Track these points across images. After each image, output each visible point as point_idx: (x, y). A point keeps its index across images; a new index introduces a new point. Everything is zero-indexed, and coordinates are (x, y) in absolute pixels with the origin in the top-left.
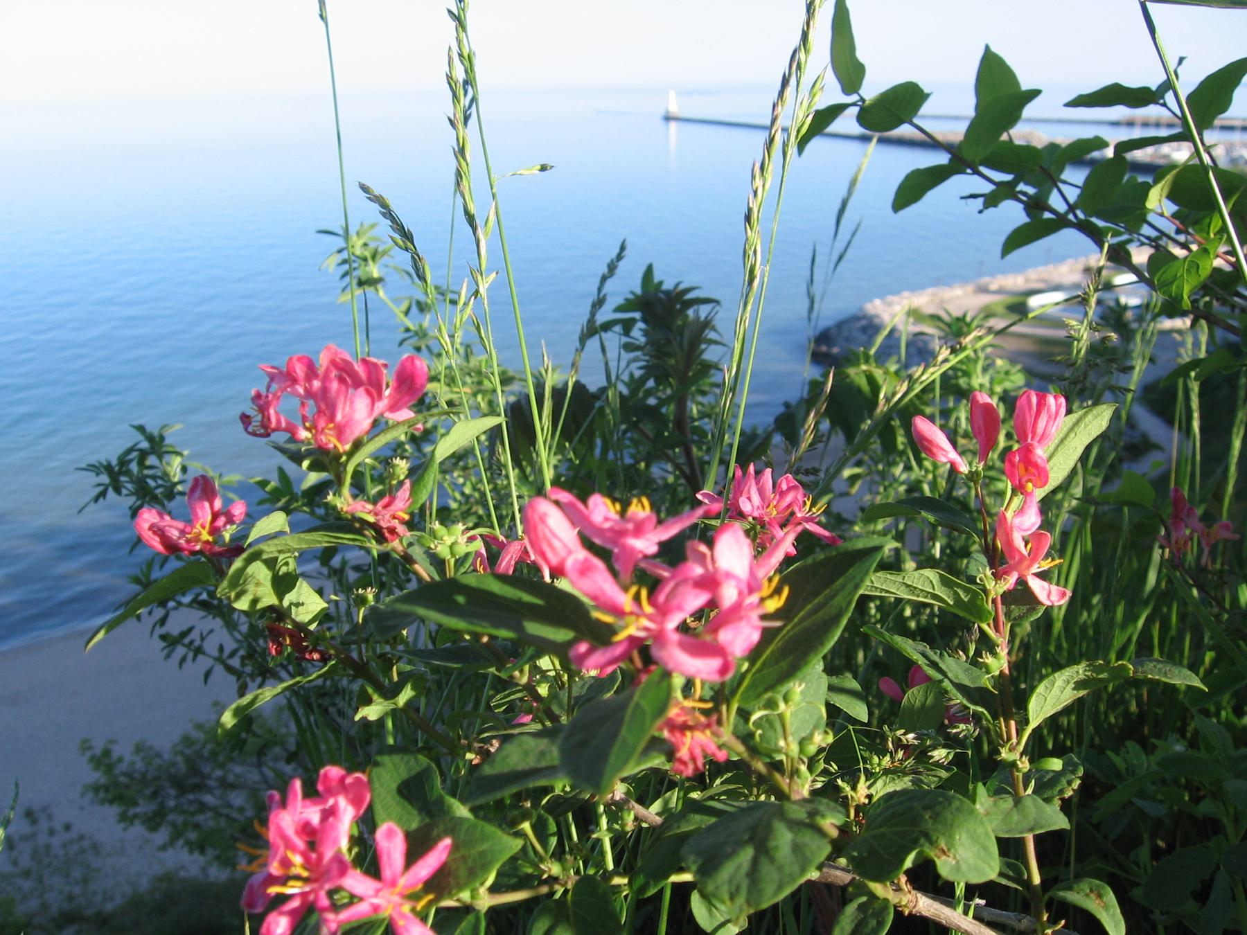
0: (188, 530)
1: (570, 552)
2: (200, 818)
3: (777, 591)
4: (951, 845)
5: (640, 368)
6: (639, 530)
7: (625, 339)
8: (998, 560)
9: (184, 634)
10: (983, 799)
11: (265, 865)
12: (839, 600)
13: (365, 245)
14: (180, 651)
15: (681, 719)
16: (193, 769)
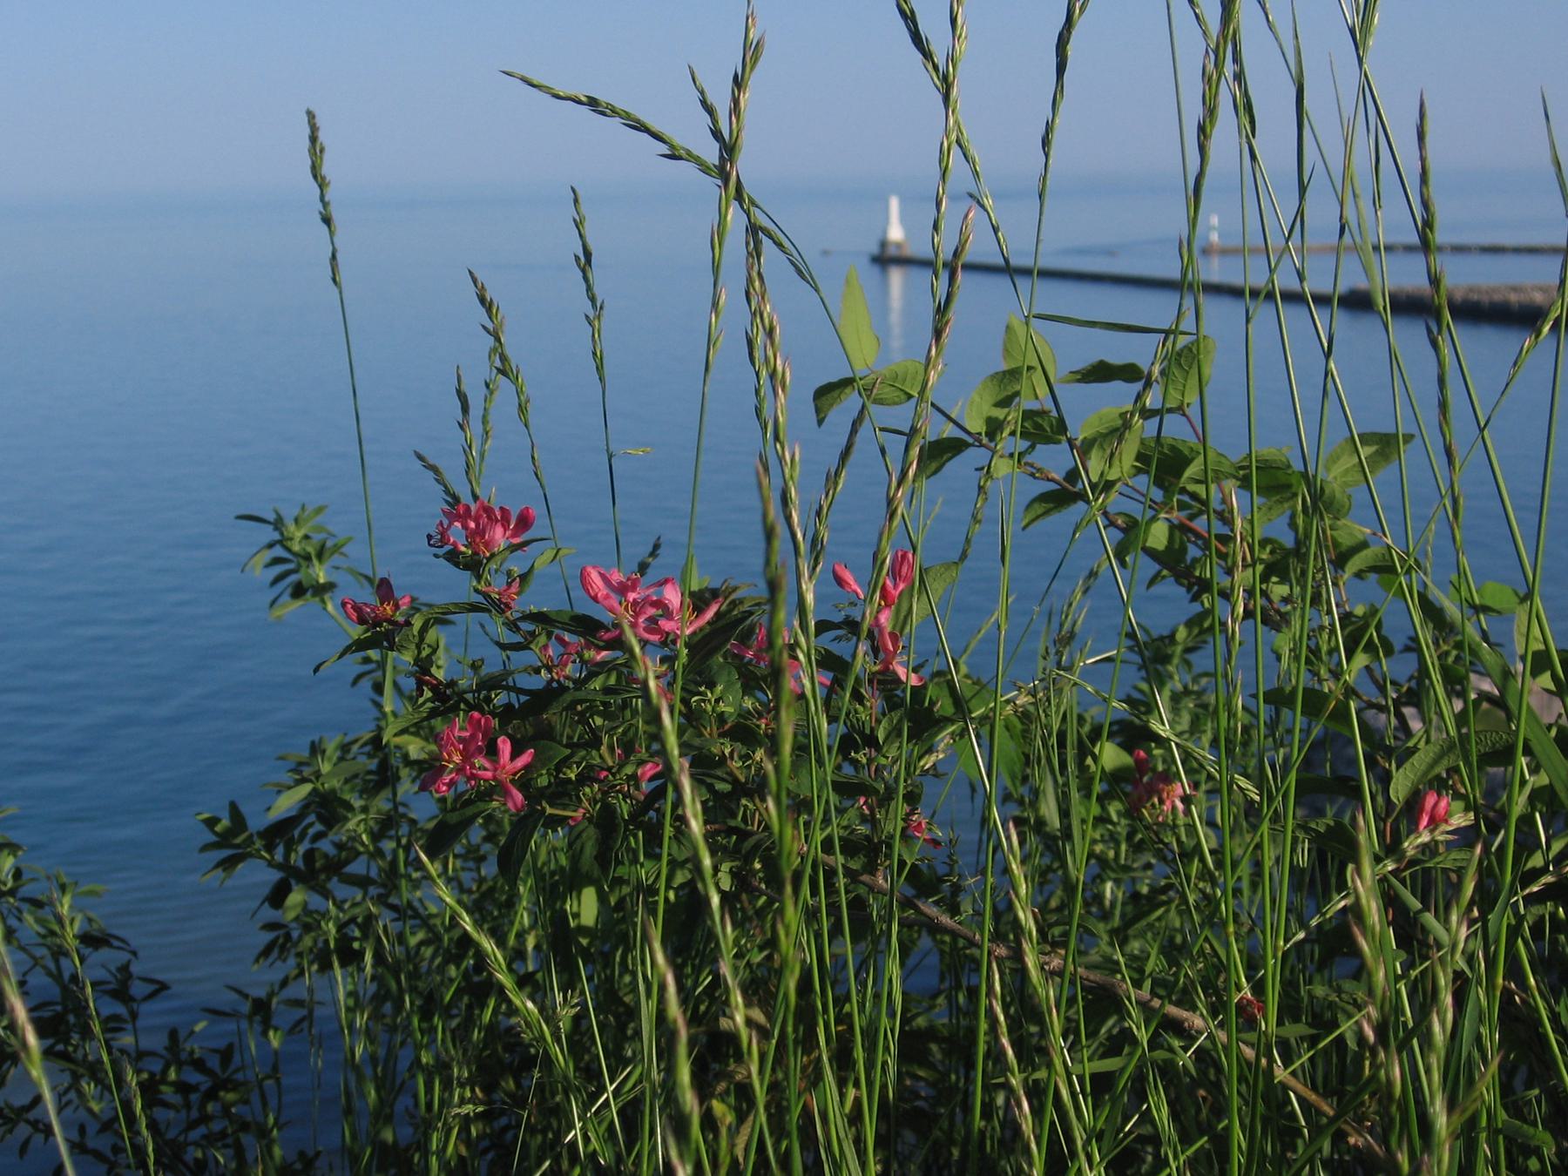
13: (306, 537)
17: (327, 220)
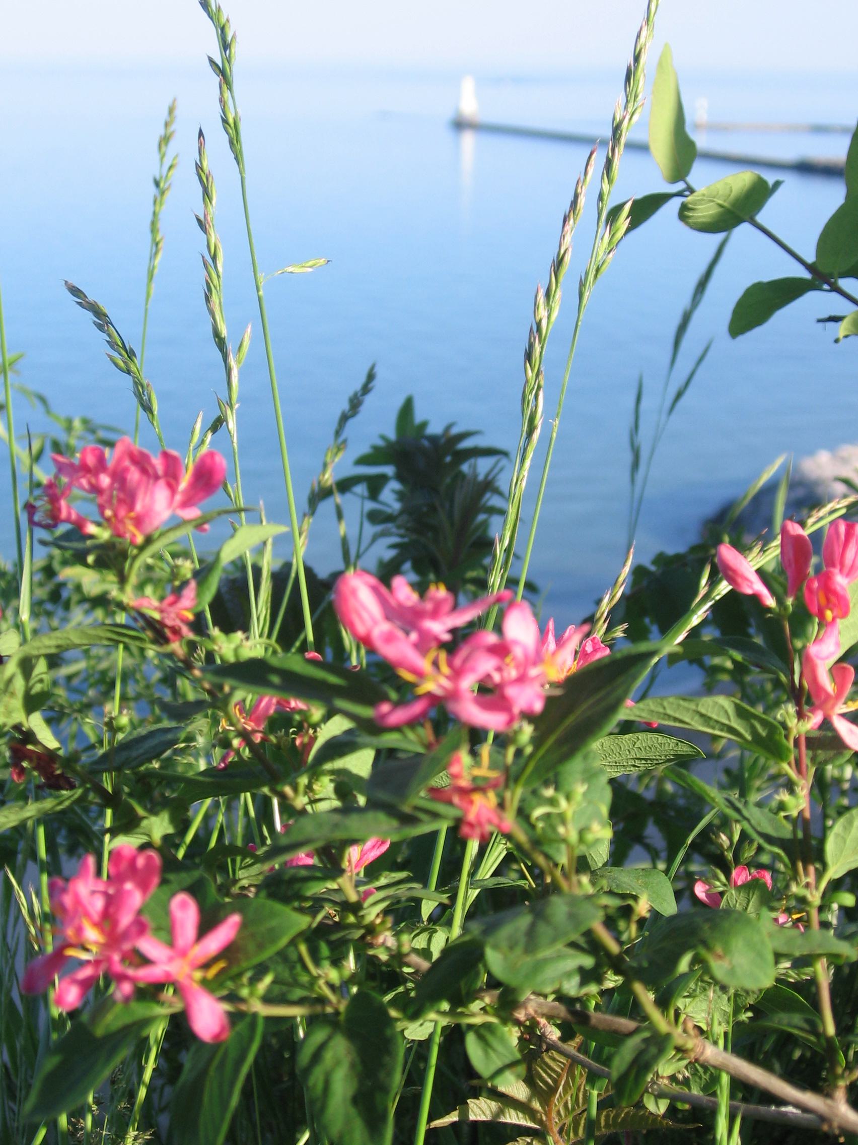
1: (375, 622)
4: (727, 950)
5: (393, 546)
6: (435, 614)
7: (370, 505)
8: (804, 698)
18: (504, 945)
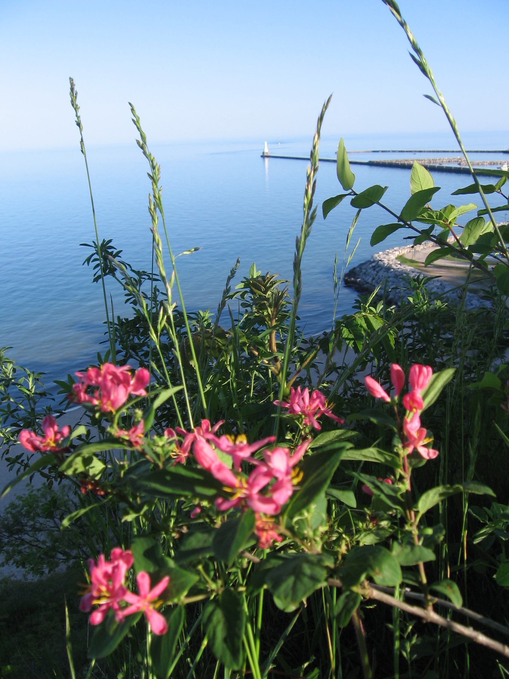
0: (44, 441)
2: (21, 548)
3: (298, 475)
4: (381, 570)
6: (241, 449)
9: (18, 457)
10: (396, 548)
11: (90, 591)
12: (326, 472)
14: (17, 466)
15: (261, 526)
16: (17, 522)
17: (79, 124)
18: (282, 596)
